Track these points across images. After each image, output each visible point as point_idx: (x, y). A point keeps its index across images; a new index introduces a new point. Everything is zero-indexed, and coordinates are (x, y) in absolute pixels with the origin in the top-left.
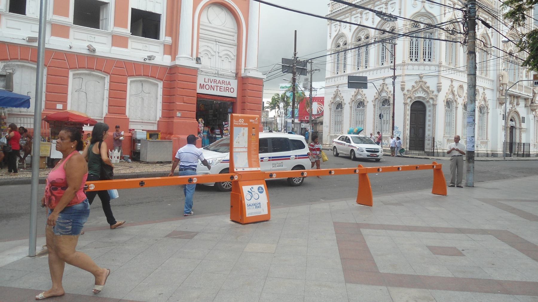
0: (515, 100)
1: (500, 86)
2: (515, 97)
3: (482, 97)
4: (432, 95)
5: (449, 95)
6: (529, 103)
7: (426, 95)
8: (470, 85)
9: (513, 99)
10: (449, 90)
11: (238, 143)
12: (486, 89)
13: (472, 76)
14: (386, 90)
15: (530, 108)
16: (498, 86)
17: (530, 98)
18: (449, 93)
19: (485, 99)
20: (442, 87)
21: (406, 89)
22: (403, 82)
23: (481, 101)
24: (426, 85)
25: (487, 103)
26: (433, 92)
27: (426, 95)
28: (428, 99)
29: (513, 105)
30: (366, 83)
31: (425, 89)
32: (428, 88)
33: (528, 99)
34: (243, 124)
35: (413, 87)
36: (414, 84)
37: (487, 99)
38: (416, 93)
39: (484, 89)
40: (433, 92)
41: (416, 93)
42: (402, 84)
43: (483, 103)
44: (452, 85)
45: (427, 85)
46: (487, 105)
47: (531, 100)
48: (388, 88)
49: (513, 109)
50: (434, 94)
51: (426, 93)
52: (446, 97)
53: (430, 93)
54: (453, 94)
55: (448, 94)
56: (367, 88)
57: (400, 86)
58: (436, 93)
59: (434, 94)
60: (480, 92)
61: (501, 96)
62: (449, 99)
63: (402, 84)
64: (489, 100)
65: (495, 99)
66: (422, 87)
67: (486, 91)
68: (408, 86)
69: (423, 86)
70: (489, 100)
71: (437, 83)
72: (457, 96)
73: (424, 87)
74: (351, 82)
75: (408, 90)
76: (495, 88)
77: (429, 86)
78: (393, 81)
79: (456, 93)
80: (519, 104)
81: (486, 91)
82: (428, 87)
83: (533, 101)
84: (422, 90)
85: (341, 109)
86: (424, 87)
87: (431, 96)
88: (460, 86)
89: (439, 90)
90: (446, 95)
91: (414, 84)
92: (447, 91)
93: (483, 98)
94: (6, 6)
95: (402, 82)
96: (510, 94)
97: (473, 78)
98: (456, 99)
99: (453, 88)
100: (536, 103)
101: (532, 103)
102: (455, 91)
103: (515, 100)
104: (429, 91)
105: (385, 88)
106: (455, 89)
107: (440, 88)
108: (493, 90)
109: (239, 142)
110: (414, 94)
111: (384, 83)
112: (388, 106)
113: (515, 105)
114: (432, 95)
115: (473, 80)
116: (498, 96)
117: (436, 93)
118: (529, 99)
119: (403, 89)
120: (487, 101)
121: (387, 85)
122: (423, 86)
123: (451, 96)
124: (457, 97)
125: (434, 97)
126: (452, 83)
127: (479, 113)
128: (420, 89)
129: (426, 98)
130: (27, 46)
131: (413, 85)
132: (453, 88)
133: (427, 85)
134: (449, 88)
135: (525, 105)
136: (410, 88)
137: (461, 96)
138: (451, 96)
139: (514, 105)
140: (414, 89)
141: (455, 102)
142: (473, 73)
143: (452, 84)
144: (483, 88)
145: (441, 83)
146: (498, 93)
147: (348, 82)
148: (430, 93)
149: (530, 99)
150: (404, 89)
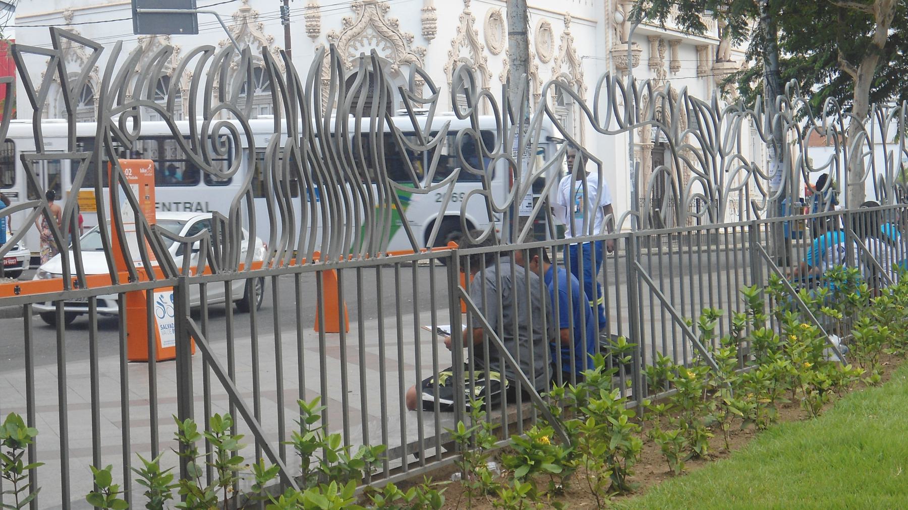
0: (667, 54)
1: (616, 9)
2: (666, 44)
3: (560, 48)
4: (408, 50)
5: (460, 47)
6: (710, 63)
7: (388, 52)
8: (514, 60)
9: (660, 51)
10: (459, 31)
11: (125, 215)
12: (573, 20)
13: (519, 37)
14: (257, 34)
15: (714, 81)
16: (610, 8)
17: (713, 45)
18: (460, 43)
19: (570, 57)
20: (438, 24)
21: (325, 31)
22: (314, 7)
23: (559, 62)
24: (386, 18)
25: (578, 70)
26: (410, 40)
27: (388, 52)
28: (396, 67)
29: (659, 73)
30: (191, 14)
31: (385, 29)
32: (392, 25)
33: (705, 47)
34: (131, 178)
35: (347, 22)
36: (349, 14)
37: (577, 56)
38: (358, 45)
39: (566, 22)
40: (410, 40)
41: (358, 45)
42: (311, 12)
43: (565, 69)
44: (468, 14)
45: (392, 15)
46: (579, 76)
47: (715, 50)
48: (260, 28)
49: (661, 84)
50: (414, 47)
51: (388, 45)
52: (450, 54)
53: (401, 44)
54: (473, 44)
55: (457, 45)
56: (197, 33)
57: (304, 23)
58: (418, 43)
59: (414, 47)
60: (554, 33)
61: (619, 42)
62: (461, 60)
63: (311, 12)
64: (582, 58)
65: (603, 53)
66: (376, 24)
67: (574, 29)
68: (330, 24)
69: (377, 19)
70: (582, 58)
71: (421, 7)
72: (486, 49)
73: (381, 25)
74: (143, 10)
75: (329, 36)
76: (601, 19)
77: (395, 18)
78: (282, 7)
79: (480, 40)
80: (678, 67)
81: (574, 29)
82: (395, 25)
83: (722, 55)
84: (374, 34)
85: (86, 105)
86: (381, 25)
87: (404, 55)
88: (491, 17)
89: (429, 35)
90: (450, 48)
91: (349, 14)
92: (454, 35)
93: (564, 52)
94: (505, 173)
95: (309, 8)
96: (649, 34)
97: (521, 43)
98: (482, 62)
99: (470, 24)
100: (729, 61)
101: (718, 60)
102: (477, 34)
103: (667, 54)
104: (397, 38)
105: (252, 28)
106: (479, 27)
107: (432, 26)
108: (596, 23)
109: (127, 213)
110: (352, 50)
111: (246, 7)
112: (264, 91)
113: (665, 71)
114: (408, 50)
115: (522, 46)
116: (610, 45)
117: (418, 43)
118: (710, 47)
119: (313, 32)
120: (576, 62)
121: (256, 16)
122: (377, 19)
123: (465, 53)
124: (486, 53)
125: (414, 58)
126: (467, 6)
127: (556, 103)
128: (370, 31)
129: (389, 60)
130: (904, 244)
131: (347, 17)
132: (470, 22)
133: (392, 15)
134: (459, 24)
135: (698, 68)
136: (338, 29)
137: (496, 51)
138: (465, 53)
139: (662, 72)
140: (350, 33)
141: (478, 71)
142: (520, 30)
143: (469, 10)
144: (562, 18)
145: (434, 9)
146: (611, 32)
147: (135, 13)
148: (401, 44)
149: (713, 49)
150: (319, 32)
